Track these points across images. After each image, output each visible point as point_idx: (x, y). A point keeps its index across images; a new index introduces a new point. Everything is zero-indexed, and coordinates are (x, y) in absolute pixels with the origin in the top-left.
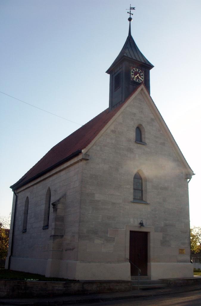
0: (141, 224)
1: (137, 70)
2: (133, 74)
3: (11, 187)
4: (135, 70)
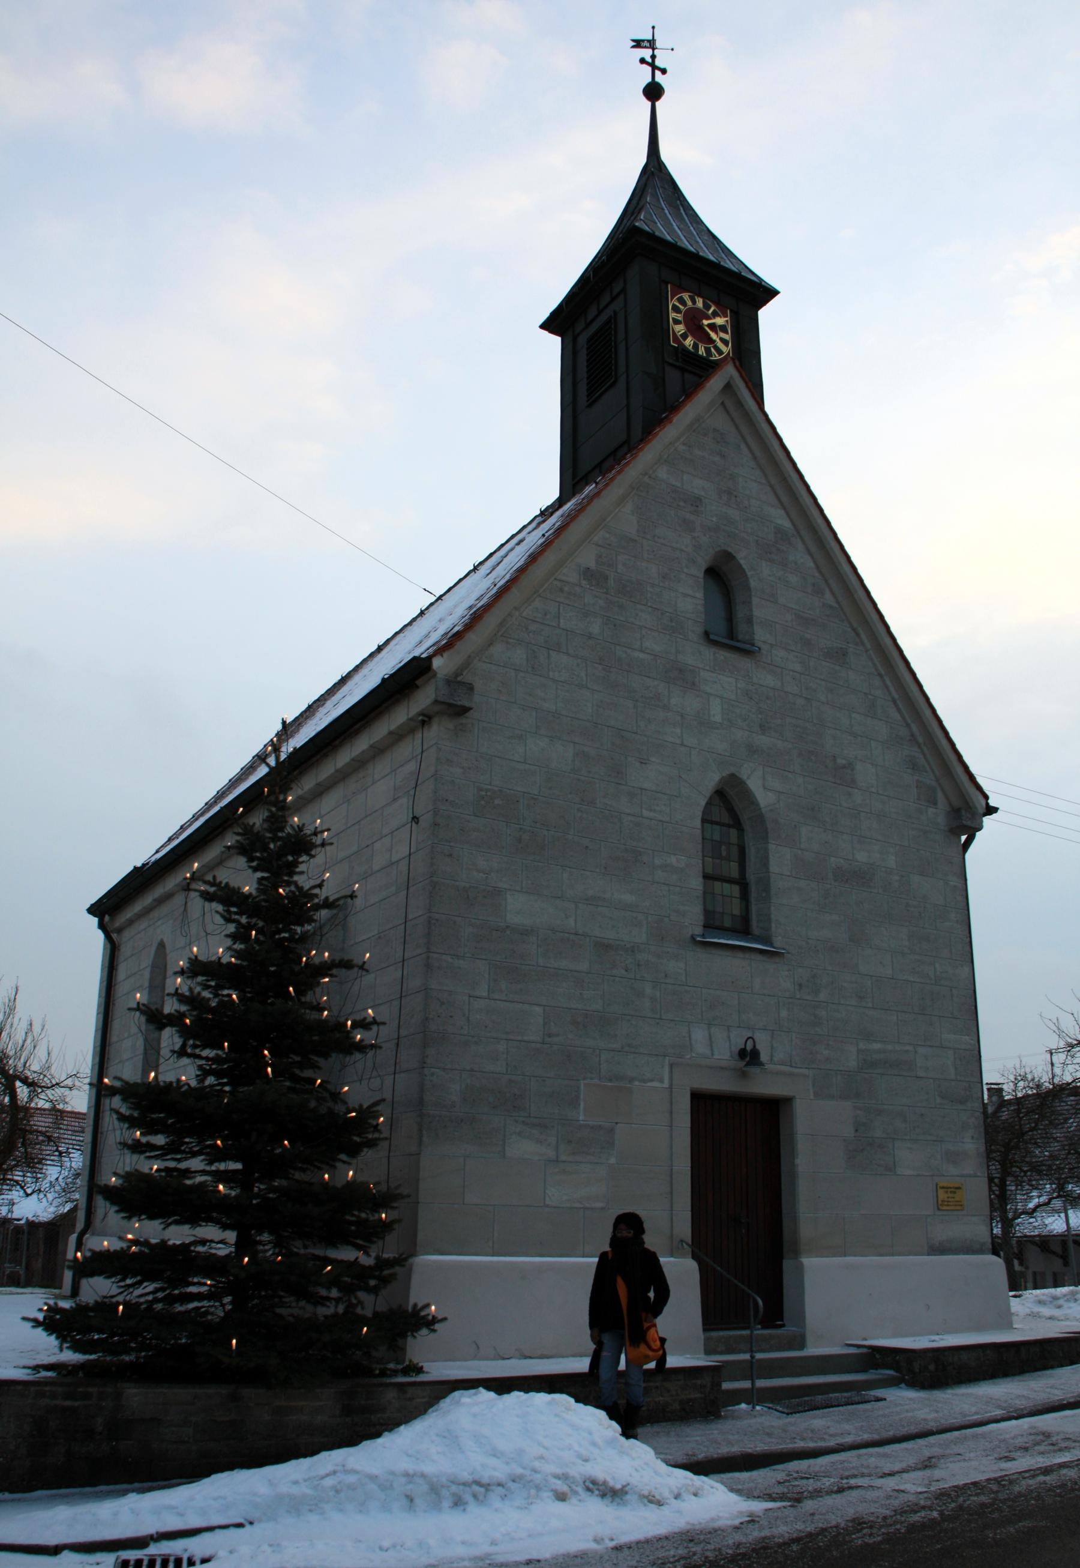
0: (749, 1056)
1: (700, 303)
2: (679, 317)
3: (93, 910)
4: (689, 303)
